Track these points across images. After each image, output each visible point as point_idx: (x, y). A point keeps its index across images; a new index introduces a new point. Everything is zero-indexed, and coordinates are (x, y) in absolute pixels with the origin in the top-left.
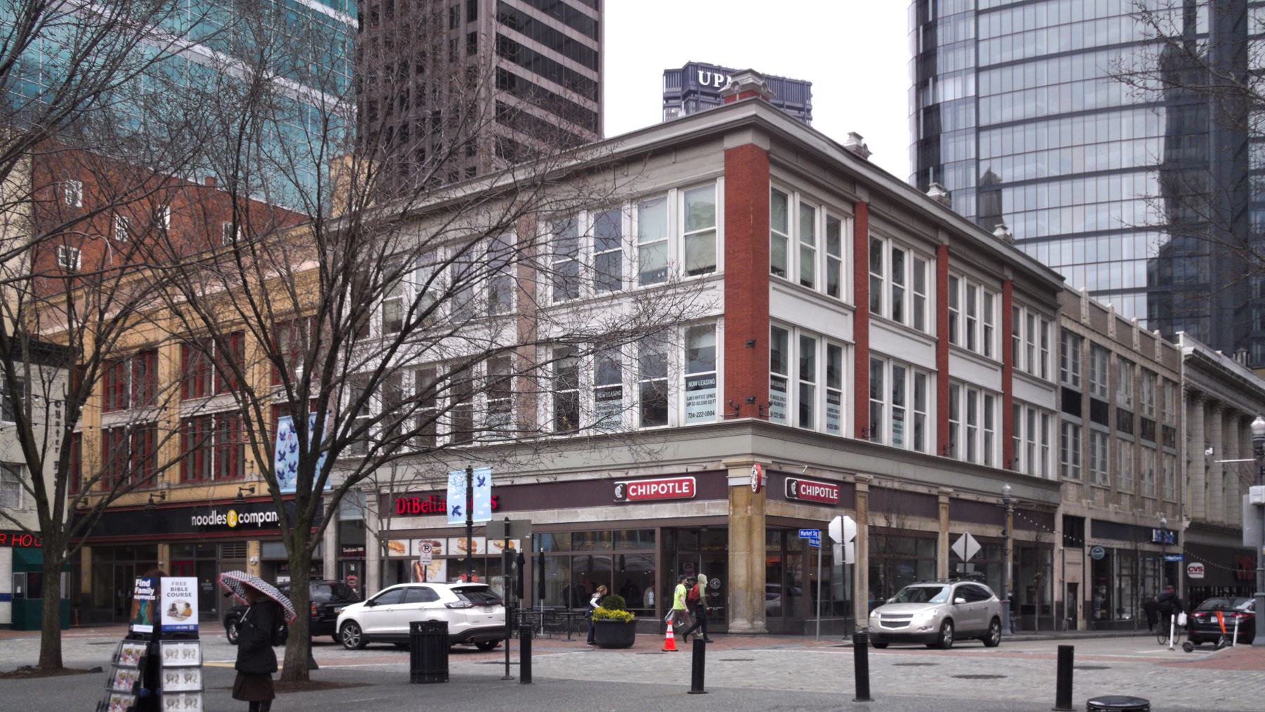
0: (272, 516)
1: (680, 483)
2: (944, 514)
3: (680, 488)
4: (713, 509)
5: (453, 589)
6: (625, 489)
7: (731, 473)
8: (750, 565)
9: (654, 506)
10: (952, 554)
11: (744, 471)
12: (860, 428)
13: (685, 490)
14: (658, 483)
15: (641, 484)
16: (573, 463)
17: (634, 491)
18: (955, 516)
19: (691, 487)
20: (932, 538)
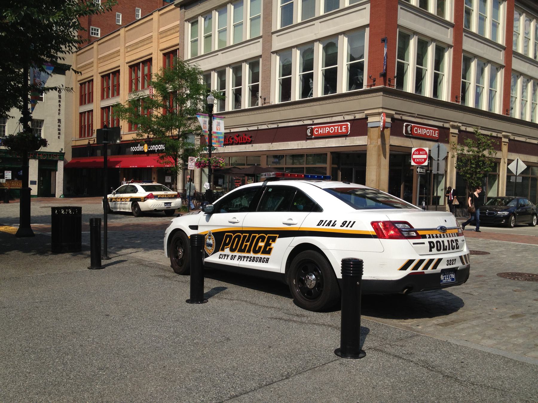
0: (162, 147)
1: (341, 126)
2: (505, 148)
3: (341, 129)
4: (359, 141)
5: (141, 186)
6: (312, 130)
7: (370, 119)
8: (379, 175)
9: (327, 140)
10: (509, 171)
11: (376, 119)
12: (454, 95)
13: (344, 130)
14: (329, 127)
15: (321, 127)
16: (289, 117)
17: (317, 131)
18: (511, 150)
19: (347, 128)
20: (496, 163)
